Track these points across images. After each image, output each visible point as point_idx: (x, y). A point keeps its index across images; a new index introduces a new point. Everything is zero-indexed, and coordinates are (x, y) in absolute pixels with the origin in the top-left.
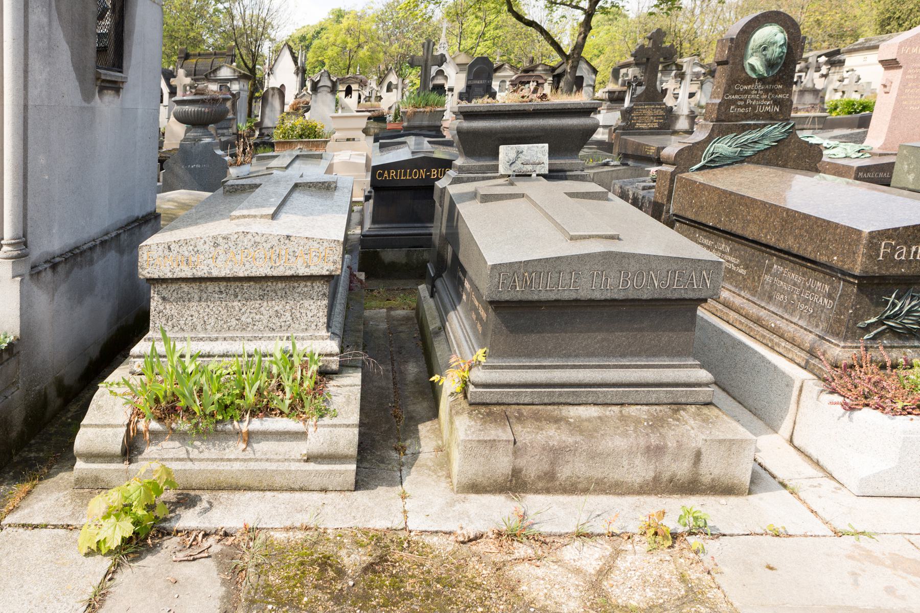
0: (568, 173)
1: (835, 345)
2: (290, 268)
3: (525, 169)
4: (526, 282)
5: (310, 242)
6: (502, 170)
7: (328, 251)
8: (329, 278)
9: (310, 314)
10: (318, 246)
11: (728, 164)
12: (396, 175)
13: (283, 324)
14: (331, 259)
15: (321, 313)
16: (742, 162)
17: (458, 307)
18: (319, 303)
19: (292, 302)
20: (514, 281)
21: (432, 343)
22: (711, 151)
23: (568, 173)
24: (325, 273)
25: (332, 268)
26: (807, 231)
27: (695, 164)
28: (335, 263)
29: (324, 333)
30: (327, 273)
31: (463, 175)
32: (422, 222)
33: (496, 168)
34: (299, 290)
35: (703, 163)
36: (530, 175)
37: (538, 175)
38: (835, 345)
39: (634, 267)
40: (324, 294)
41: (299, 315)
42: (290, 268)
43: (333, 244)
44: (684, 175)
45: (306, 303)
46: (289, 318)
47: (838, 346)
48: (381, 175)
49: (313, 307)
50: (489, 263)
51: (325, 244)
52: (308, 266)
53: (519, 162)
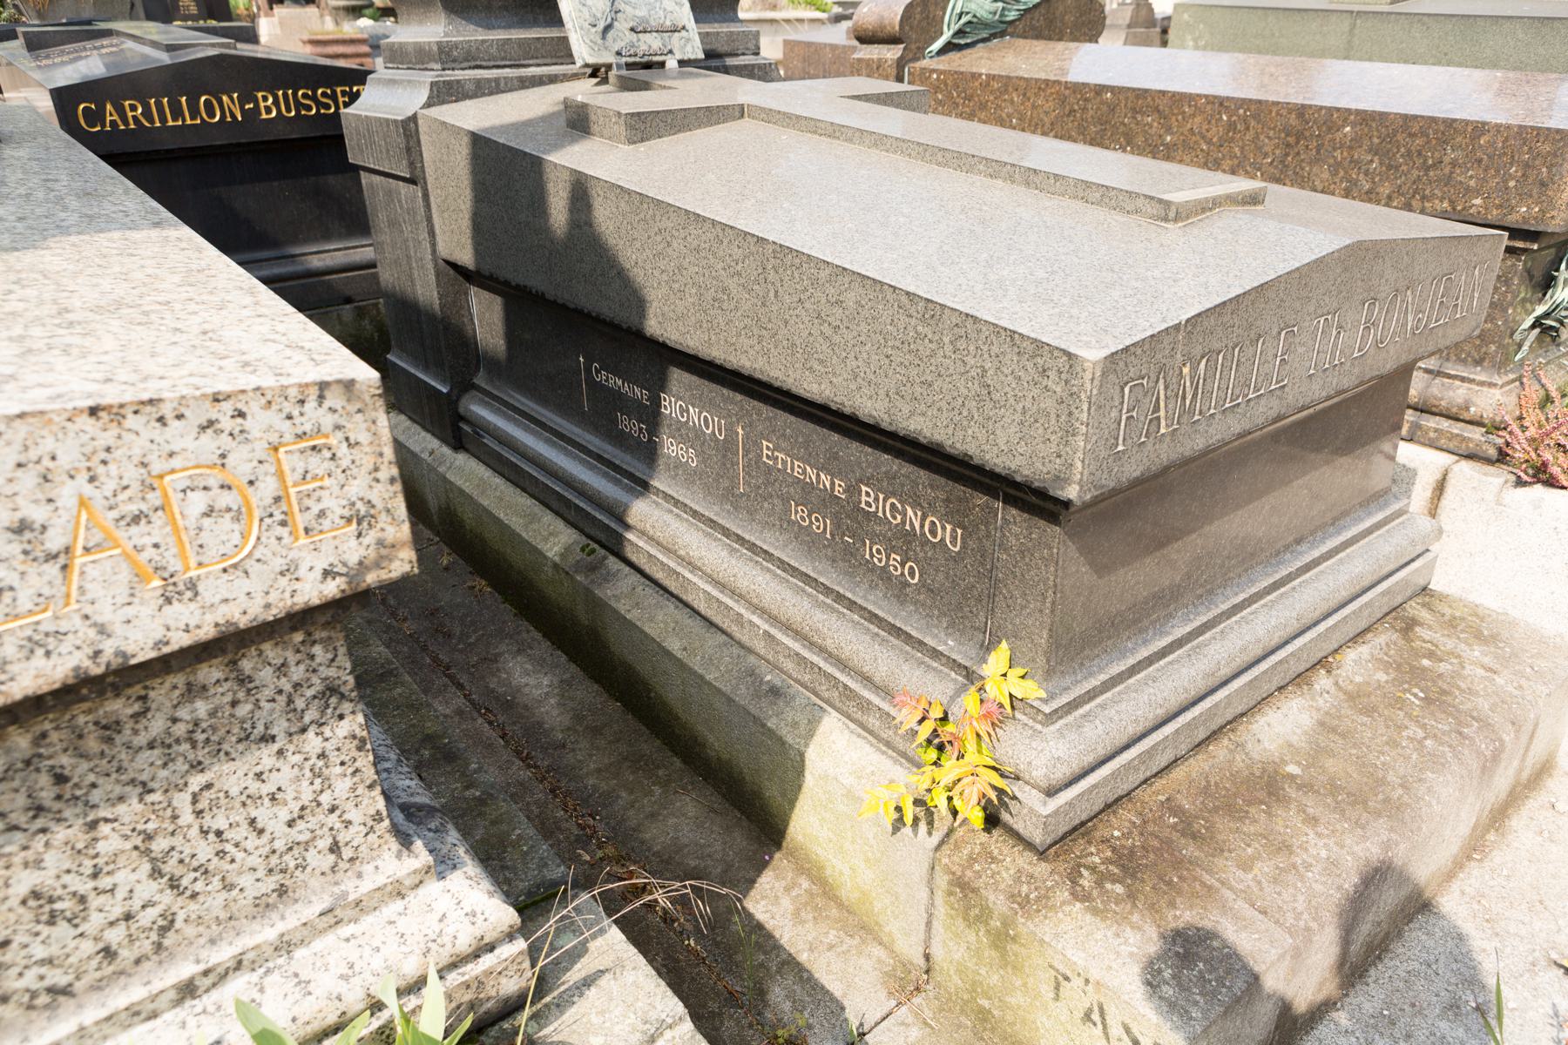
0: (730, 61)
1: (1482, 384)
2: (32, 646)
3: (643, 48)
4: (1184, 398)
5: (141, 435)
6: (583, 51)
7: (292, 463)
8: (350, 612)
9: (273, 819)
10: (209, 445)
11: (984, 40)
12: (147, 113)
13: (115, 936)
14: (335, 506)
15: (342, 786)
16: (1002, 34)
17: (655, 483)
18: (312, 742)
19: (130, 810)
20: (1156, 409)
21: (598, 606)
22: (958, 10)
23: (730, 61)
24: (314, 590)
25: (353, 551)
26: (1374, 151)
27: (934, 40)
28: (360, 519)
29: (393, 863)
30: (332, 589)
31: (459, 75)
32: (276, 244)
33: (562, 51)
34: (157, 725)
35: (946, 36)
36: (662, 65)
37: (682, 63)
38: (1482, 384)
39: (1297, 275)
40: (331, 690)
41: (204, 850)
42: (32, 646)
43: (314, 415)
44: (918, 65)
45: (232, 776)
46: (148, 889)
47: (1491, 385)
48: (95, 117)
49: (284, 776)
50: (1092, 354)
51: (260, 421)
52: (176, 590)
53: (622, 26)
